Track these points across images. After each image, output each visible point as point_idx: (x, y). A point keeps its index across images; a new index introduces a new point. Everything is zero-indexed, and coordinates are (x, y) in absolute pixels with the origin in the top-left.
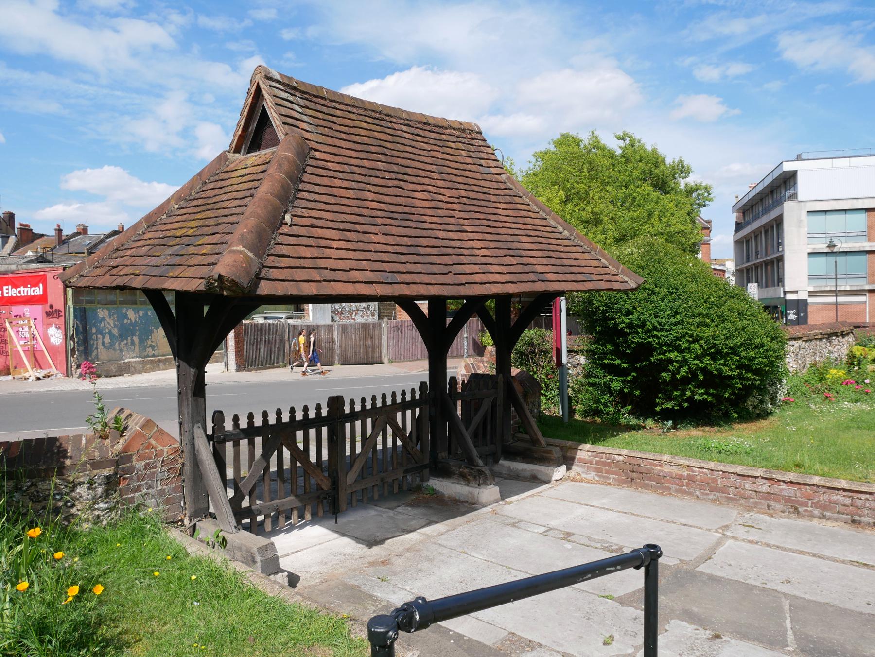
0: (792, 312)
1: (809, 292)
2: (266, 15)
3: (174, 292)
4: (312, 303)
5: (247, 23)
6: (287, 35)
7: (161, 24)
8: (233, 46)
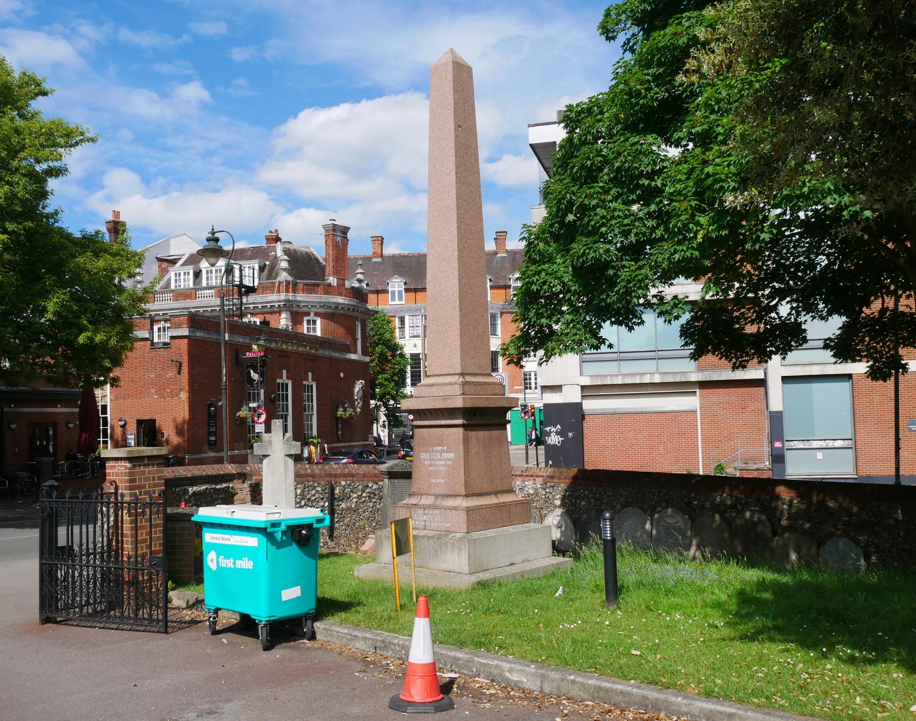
0: (553, 429)
1: (582, 387)
2: (212, 29)
3: (300, 453)
4: (698, 475)
5: (185, 39)
6: (238, 55)
7: (67, 38)
8: (163, 68)
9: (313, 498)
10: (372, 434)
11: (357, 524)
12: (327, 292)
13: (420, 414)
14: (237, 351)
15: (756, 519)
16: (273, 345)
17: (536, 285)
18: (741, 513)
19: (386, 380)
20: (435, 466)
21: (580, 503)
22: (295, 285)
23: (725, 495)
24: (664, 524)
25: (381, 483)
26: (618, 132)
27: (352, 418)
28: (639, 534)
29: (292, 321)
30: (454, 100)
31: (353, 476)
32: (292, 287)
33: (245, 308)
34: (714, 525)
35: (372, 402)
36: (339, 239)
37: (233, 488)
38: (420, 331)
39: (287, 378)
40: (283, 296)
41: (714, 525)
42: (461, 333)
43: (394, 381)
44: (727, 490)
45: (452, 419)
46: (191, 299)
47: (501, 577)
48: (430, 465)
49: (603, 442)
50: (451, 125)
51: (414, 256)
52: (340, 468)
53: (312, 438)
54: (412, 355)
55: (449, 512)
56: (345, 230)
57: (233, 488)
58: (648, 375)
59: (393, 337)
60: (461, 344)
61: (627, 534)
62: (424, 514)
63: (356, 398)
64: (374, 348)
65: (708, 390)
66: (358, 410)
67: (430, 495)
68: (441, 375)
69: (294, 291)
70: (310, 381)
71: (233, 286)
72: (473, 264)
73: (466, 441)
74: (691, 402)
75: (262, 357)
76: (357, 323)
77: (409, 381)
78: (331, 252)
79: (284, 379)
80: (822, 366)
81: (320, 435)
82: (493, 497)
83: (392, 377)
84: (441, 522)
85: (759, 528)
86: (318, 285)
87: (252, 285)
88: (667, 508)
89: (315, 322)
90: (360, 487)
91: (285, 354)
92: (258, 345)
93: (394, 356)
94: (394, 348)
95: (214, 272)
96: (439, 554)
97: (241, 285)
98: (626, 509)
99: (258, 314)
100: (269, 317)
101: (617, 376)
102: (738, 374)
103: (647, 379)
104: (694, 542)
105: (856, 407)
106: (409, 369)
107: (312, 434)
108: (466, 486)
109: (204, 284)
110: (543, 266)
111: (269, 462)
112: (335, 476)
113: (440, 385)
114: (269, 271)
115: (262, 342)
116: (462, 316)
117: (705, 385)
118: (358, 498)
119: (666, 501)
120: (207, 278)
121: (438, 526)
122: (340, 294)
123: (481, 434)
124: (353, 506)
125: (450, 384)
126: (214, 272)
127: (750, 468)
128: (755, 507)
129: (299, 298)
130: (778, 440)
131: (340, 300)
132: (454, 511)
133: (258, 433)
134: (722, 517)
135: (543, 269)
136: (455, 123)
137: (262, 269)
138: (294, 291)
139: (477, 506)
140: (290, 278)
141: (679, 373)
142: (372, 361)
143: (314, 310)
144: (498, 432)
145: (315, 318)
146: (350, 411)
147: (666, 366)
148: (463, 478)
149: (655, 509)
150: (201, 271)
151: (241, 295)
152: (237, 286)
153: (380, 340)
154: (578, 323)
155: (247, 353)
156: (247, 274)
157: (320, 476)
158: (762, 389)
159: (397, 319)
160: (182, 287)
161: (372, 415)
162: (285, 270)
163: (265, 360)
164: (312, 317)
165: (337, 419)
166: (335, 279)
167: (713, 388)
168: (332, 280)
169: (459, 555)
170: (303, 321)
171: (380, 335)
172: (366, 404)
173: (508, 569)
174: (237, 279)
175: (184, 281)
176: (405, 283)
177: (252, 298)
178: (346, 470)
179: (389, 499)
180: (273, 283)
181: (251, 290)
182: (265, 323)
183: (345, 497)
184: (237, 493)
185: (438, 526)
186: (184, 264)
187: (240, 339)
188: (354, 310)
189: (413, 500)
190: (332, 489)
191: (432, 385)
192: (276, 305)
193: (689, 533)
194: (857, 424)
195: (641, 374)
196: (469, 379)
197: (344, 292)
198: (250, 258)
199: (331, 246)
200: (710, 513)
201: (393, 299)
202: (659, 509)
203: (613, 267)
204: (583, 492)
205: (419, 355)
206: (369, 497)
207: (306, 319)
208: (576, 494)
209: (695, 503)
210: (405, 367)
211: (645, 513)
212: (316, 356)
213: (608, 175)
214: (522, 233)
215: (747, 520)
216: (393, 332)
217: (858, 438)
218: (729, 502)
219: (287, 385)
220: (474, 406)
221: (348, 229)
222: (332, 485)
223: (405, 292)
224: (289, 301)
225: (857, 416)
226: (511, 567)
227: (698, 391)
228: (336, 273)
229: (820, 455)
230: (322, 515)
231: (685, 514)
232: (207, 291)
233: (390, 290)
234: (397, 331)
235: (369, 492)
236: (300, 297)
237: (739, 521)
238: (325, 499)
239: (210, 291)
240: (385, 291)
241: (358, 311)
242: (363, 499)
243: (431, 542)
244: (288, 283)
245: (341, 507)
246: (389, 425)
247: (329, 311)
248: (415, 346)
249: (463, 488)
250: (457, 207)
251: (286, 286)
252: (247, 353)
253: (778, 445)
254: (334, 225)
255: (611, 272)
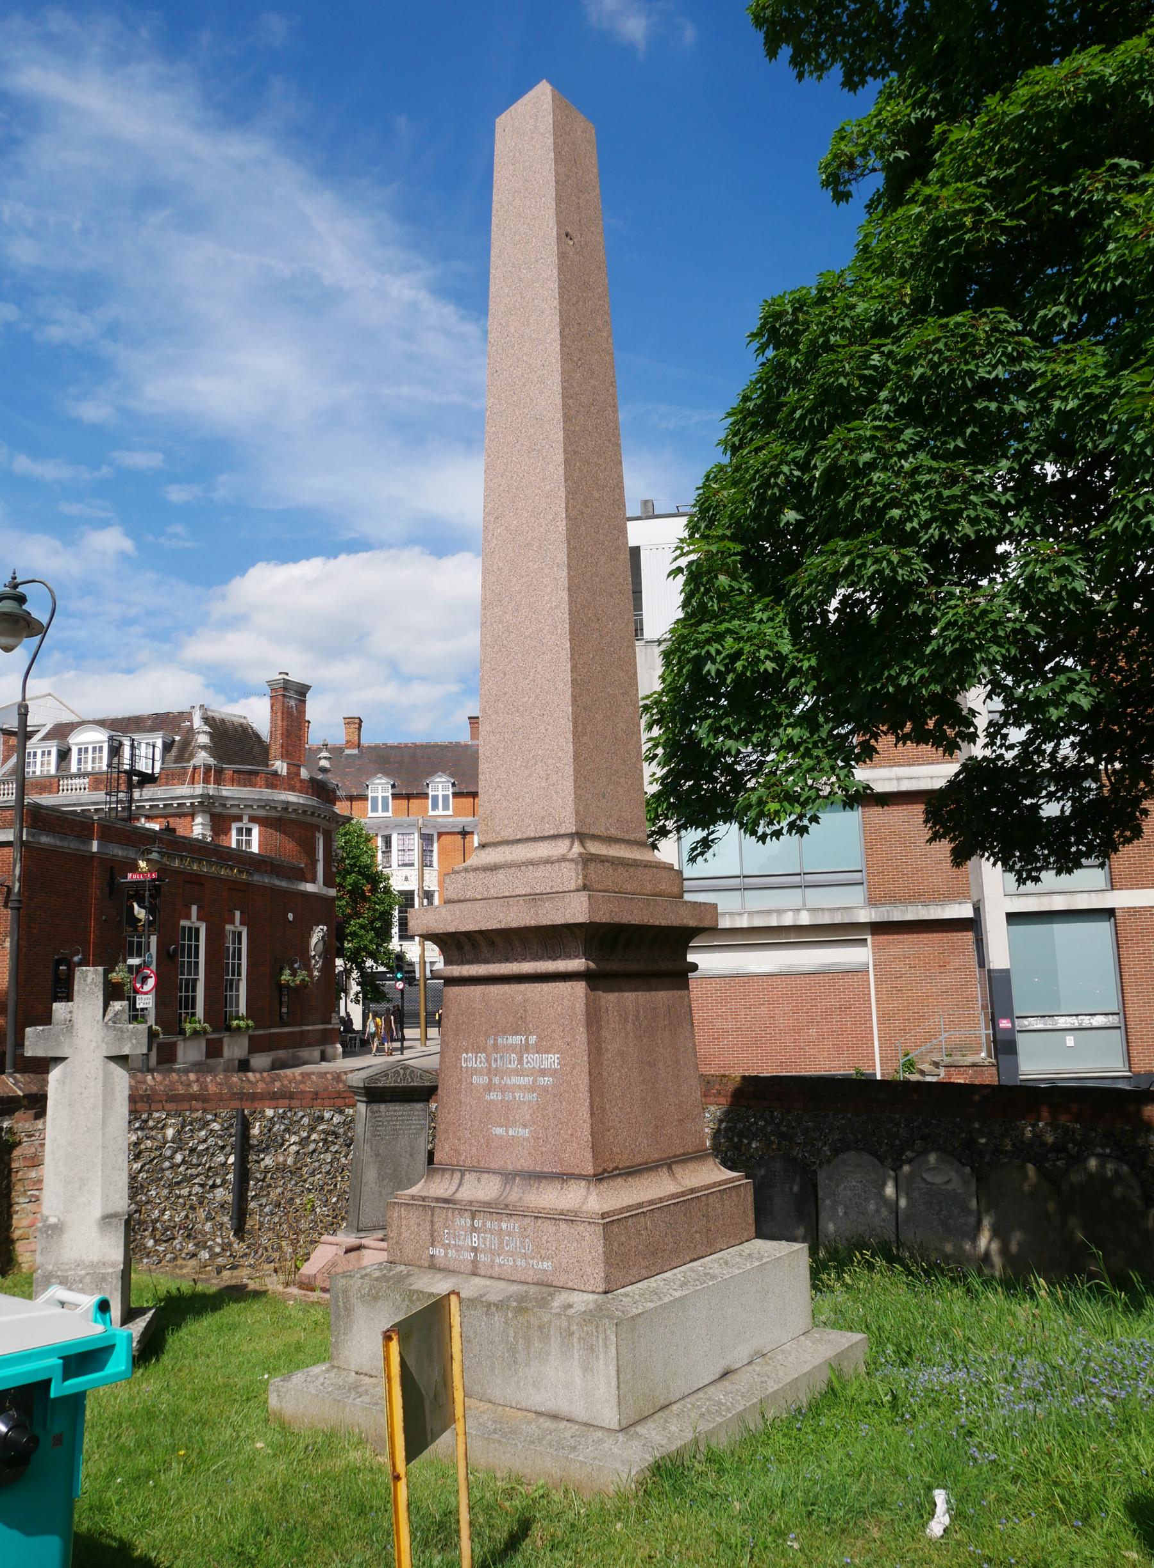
9: (201, 1147)
10: (338, 1012)
11: (298, 1201)
12: (270, 786)
13: (460, 947)
14: (114, 869)
15: (1109, 1174)
16: (177, 863)
17: (714, 662)
18: (1078, 1159)
19: (362, 927)
20: (504, 1089)
21: (749, 1144)
22: (219, 772)
23: (1041, 1124)
24: (922, 1185)
25: (350, 1111)
26: (901, 320)
27: (306, 986)
28: (872, 1207)
29: (212, 830)
30: (557, 174)
31: (291, 1096)
32: (214, 775)
33: (137, 807)
34: (1026, 1187)
35: (339, 962)
36: (292, 703)
37: (10, 1130)
38: (415, 857)
39: (199, 919)
40: (199, 789)
41: (1026, 1187)
42: (575, 725)
43: (374, 929)
44: (1045, 1114)
45: (554, 958)
46: (50, 792)
47: (712, 1432)
48: (489, 1088)
49: (718, 1023)
50: (549, 229)
51: (406, 746)
52: (263, 1079)
53: (238, 1018)
54: (401, 893)
55: (549, 1227)
56: (302, 691)
57: (10, 1130)
58: (790, 913)
59: (374, 863)
60: (576, 756)
61: (846, 1207)
62: (474, 1229)
63: (313, 953)
64: (344, 878)
65: (886, 937)
66: (316, 973)
67: (488, 1171)
68: (519, 841)
69: (218, 782)
70: (237, 926)
71: (119, 772)
72: (603, 559)
73: (593, 1019)
74: (860, 955)
75: (154, 880)
76: (317, 835)
77: (395, 930)
78: (279, 722)
79: (193, 920)
80: (1068, 896)
81: (250, 1014)
82: (664, 1174)
83: (372, 922)
84: (524, 1256)
85: (1118, 1191)
86: (255, 773)
87: (150, 772)
88: (925, 1152)
89: (249, 831)
90: (306, 1121)
91: (197, 880)
92: (148, 861)
93: (374, 890)
94: (375, 879)
95: (90, 750)
96: (521, 1357)
97: (132, 772)
98: (845, 1156)
99: (157, 817)
100: (174, 822)
101: (740, 914)
102: (932, 911)
103: (788, 920)
104: (986, 1223)
105: (1124, 961)
106: (396, 913)
107: (238, 1011)
108: (597, 1147)
109: (74, 768)
110: (726, 625)
111: (64, 1075)
112: (253, 1097)
113: (518, 865)
114: (179, 751)
115: (154, 856)
116: (578, 685)
117: (879, 928)
118: (299, 1143)
119: (923, 1138)
120: (79, 761)
121: (515, 1267)
122: (292, 789)
123: (630, 999)
124: (290, 1161)
125: (548, 861)
126: (90, 750)
127: (961, 1063)
128: (1103, 1147)
129: (225, 793)
130: (1005, 1018)
131: (292, 797)
132: (563, 1226)
133: (143, 1010)
134: (1039, 1169)
135: (729, 631)
136: (559, 223)
137: (167, 747)
138: (218, 782)
139: (629, 1208)
140: (211, 761)
141: (839, 909)
142: (340, 898)
143: (250, 811)
144: (669, 993)
145: (250, 825)
146: (302, 975)
147: (817, 898)
148: (587, 1127)
149: (902, 1154)
150: (70, 749)
151: (130, 787)
152: (125, 772)
153: (353, 865)
154: (815, 745)
155: (130, 875)
156: (143, 754)
157: (220, 1098)
158: (970, 936)
159: (379, 839)
160: (38, 773)
161: (338, 984)
162: (204, 747)
163: (159, 886)
164: (245, 823)
165: (281, 988)
166: (285, 765)
167: (893, 933)
168: (280, 766)
169: (587, 1369)
170: (230, 829)
171: (353, 858)
172: (329, 965)
173: (718, 1393)
174: (126, 760)
175: (42, 764)
176: (393, 786)
177: (149, 792)
178: (277, 1084)
179: (367, 1148)
180: (184, 768)
181: (148, 779)
182: (169, 830)
183: (274, 1143)
184: (20, 1143)
185: (515, 1267)
186: (43, 739)
187: (118, 851)
188: (313, 814)
189: (440, 1187)
190: (246, 1126)
191: (493, 868)
192: (188, 802)
193: (974, 1204)
194: (1127, 989)
195: (780, 912)
196: (595, 848)
197: (298, 785)
198: (151, 730)
199: (279, 714)
200: (1017, 1162)
201: (374, 809)
202: (909, 1154)
203: (921, 596)
204: (756, 1123)
205: (412, 893)
206: (325, 1141)
207: (234, 826)
208: (740, 1125)
209: (983, 1141)
210: (392, 909)
211: (882, 1162)
212: (248, 884)
213: (891, 401)
214: (676, 559)
215: (1091, 1176)
216: (373, 856)
217: (1129, 1010)
218: (1050, 1139)
219: (197, 930)
220: (616, 920)
221: (308, 688)
222: (244, 1116)
223: (393, 798)
224: (210, 797)
225: (1126, 976)
226: (726, 1382)
227: (869, 938)
228: (286, 755)
229: (1070, 1040)
230: (99, 1328)
231: (964, 1165)
232: (77, 781)
233: (370, 795)
234: (380, 855)
235: (323, 1131)
236: (227, 791)
237: (1076, 1178)
238: (228, 1149)
239: (82, 781)
240: (364, 798)
241: (319, 815)
242: (312, 1146)
243: (498, 1319)
244: (208, 768)
245: (263, 1164)
246: (364, 998)
247: (273, 814)
248: (406, 879)
249: (589, 1155)
250: (565, 415)
251: (205, 773)
252: (130, 875)
253: (1004, 1024)
254: (286, 681)
255: (916, 608)
